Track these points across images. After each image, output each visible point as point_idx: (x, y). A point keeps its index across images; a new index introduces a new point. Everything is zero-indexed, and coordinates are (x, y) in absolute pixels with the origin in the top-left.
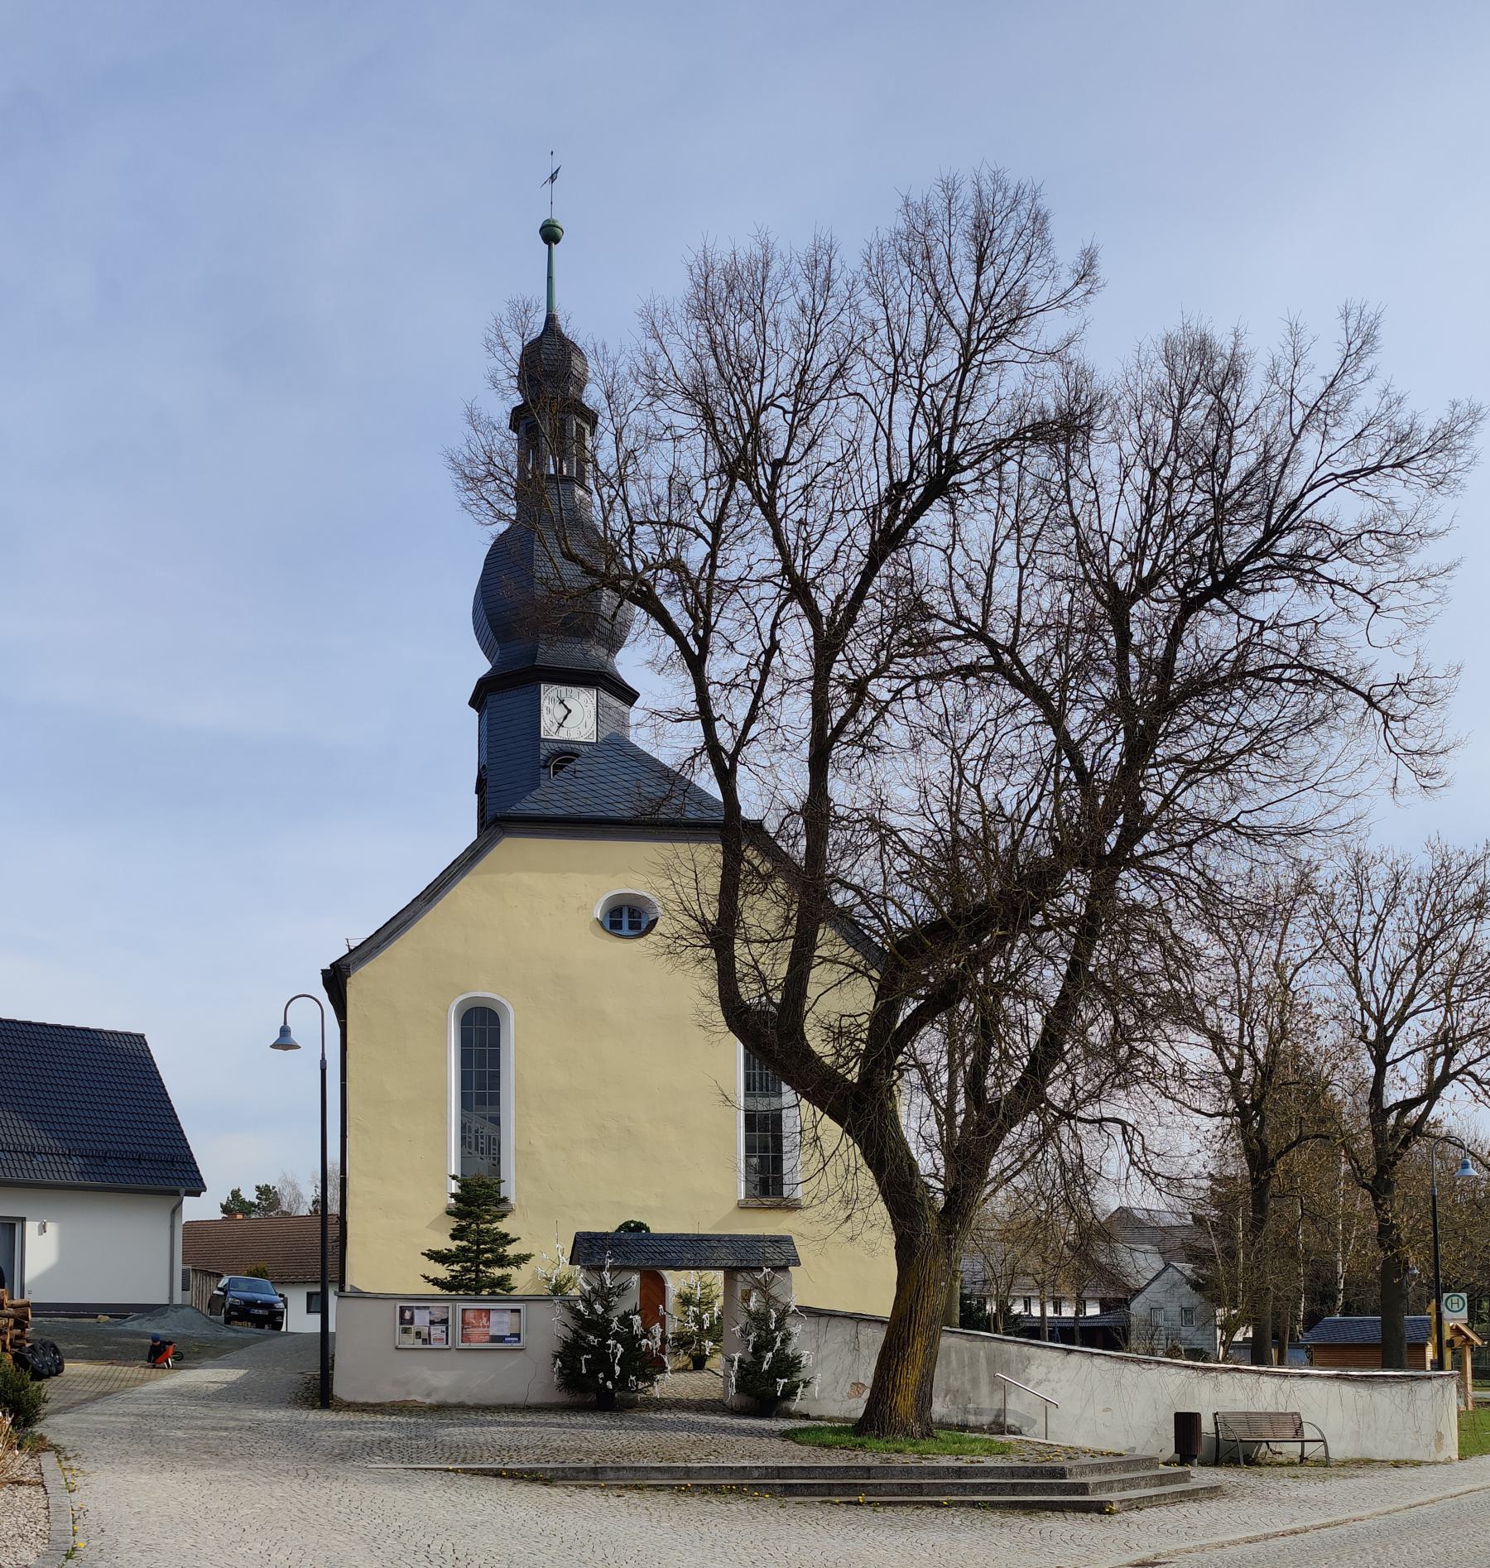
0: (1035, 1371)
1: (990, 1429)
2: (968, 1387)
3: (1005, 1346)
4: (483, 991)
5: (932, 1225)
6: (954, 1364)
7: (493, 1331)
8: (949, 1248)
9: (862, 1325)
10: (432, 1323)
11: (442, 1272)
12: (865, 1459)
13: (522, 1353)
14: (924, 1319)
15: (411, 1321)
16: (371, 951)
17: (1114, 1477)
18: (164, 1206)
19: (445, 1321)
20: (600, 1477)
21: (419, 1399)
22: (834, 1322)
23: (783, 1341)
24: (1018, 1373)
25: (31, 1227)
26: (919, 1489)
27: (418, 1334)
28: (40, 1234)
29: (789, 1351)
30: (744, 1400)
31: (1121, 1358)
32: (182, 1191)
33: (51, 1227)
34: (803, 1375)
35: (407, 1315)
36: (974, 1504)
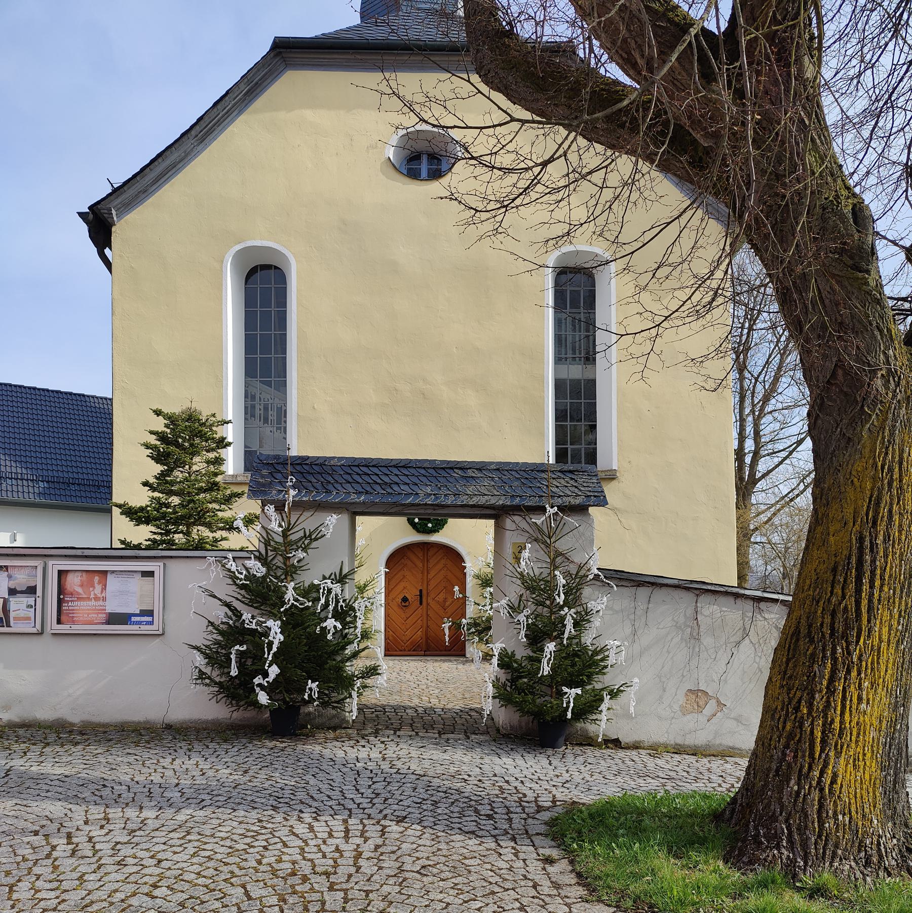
7: (113, 606)
9: (704, 599)
10: (12, 592)
13: (157, 640)
19: (31, 590)
22: (660, 594)
23: (576, 624)
29: (587, 639)
30: (504, 717)
34: (610, 679)
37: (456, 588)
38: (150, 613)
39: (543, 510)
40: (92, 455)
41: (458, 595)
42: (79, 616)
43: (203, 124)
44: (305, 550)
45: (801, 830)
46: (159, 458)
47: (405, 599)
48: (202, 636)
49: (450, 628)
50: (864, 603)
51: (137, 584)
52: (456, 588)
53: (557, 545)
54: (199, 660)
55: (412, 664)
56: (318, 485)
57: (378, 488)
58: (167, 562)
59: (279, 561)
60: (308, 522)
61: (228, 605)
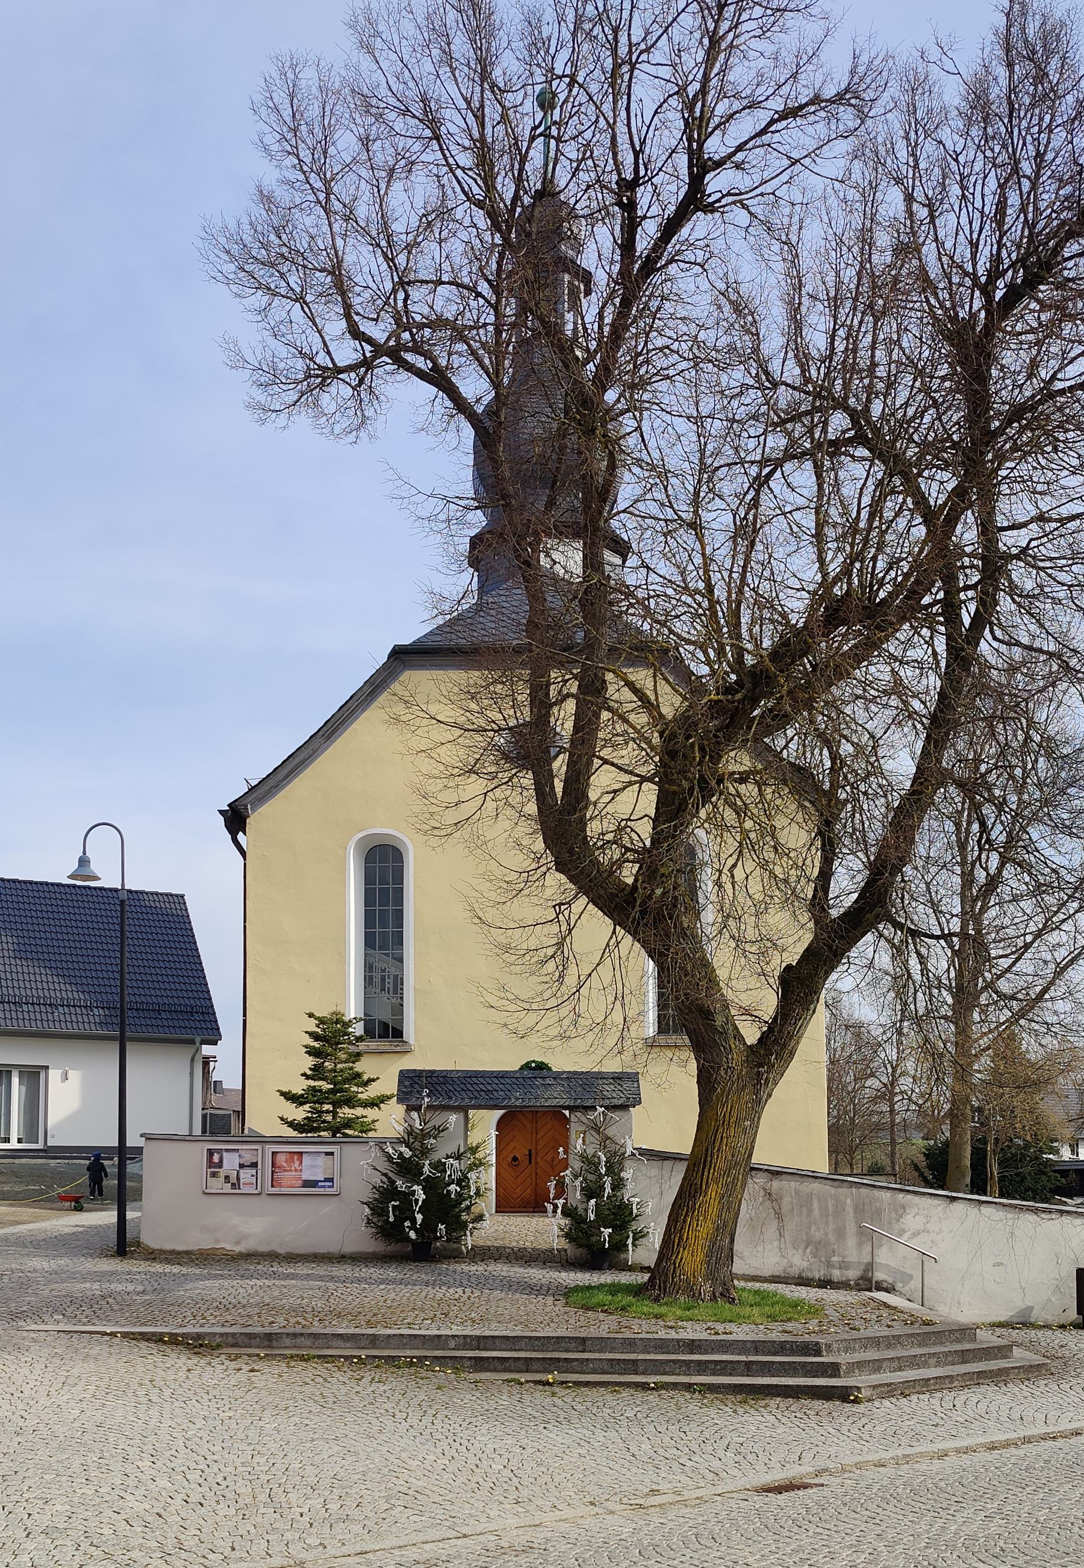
0: (911, 1221)
1: (857, 1284)
2: (832, 1238)
3: (876, 1193)
4: (384, 828)
5: (736, 1058)
6: (816, 1212)
7: (307, 1176)
8: (759, 1082)
10: (242, 1166)
11: (299, 1113)
12: (641, 1328)
14: (721, 1164)
15: (220, 1165)
16: (269, 791)
17: (900, 1352)
18: (188, 1051)
19: (254, 1165)
20: (275, 1344)
21: (228, 1247)
24: (890, 1223)
25: (54, 1075)
26: (633, 1367)
27: (227, 1178)
28: (63, 1081)
31: (1015, 1207)
32: (198, 1040)
33: (71, 1074)
35: (216, 1158)
36: (689, 1387)
37: (561, 1149)
38: (331, 1180)
39: (594, 1108)
40: (52, 895)
41: (562, 1155)
42: (284, 1182)
43: (329, 725)
44: (435, 1138)
45: (665, 1283)
46: (312, 1052)
47: (515, 1159)
48: (368, 1195)
49: (556, 1185)
50: (705, 1180)
51: (321, 1161)
52: (561, 1149)
53: (606, 1132)
54: (367, 1211)
55: (519, 1219)
56: (443, 1093)
57: (483, 1093)
58: (343, 1145)
59: (417, 1145)
60: (437, 1120)
61: (385, 1175)
